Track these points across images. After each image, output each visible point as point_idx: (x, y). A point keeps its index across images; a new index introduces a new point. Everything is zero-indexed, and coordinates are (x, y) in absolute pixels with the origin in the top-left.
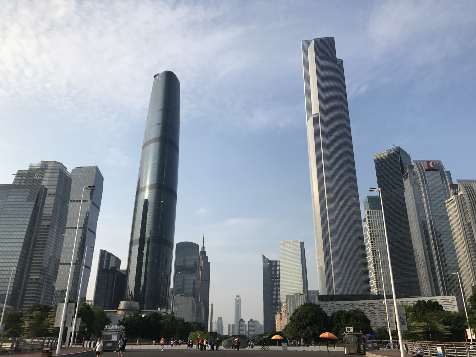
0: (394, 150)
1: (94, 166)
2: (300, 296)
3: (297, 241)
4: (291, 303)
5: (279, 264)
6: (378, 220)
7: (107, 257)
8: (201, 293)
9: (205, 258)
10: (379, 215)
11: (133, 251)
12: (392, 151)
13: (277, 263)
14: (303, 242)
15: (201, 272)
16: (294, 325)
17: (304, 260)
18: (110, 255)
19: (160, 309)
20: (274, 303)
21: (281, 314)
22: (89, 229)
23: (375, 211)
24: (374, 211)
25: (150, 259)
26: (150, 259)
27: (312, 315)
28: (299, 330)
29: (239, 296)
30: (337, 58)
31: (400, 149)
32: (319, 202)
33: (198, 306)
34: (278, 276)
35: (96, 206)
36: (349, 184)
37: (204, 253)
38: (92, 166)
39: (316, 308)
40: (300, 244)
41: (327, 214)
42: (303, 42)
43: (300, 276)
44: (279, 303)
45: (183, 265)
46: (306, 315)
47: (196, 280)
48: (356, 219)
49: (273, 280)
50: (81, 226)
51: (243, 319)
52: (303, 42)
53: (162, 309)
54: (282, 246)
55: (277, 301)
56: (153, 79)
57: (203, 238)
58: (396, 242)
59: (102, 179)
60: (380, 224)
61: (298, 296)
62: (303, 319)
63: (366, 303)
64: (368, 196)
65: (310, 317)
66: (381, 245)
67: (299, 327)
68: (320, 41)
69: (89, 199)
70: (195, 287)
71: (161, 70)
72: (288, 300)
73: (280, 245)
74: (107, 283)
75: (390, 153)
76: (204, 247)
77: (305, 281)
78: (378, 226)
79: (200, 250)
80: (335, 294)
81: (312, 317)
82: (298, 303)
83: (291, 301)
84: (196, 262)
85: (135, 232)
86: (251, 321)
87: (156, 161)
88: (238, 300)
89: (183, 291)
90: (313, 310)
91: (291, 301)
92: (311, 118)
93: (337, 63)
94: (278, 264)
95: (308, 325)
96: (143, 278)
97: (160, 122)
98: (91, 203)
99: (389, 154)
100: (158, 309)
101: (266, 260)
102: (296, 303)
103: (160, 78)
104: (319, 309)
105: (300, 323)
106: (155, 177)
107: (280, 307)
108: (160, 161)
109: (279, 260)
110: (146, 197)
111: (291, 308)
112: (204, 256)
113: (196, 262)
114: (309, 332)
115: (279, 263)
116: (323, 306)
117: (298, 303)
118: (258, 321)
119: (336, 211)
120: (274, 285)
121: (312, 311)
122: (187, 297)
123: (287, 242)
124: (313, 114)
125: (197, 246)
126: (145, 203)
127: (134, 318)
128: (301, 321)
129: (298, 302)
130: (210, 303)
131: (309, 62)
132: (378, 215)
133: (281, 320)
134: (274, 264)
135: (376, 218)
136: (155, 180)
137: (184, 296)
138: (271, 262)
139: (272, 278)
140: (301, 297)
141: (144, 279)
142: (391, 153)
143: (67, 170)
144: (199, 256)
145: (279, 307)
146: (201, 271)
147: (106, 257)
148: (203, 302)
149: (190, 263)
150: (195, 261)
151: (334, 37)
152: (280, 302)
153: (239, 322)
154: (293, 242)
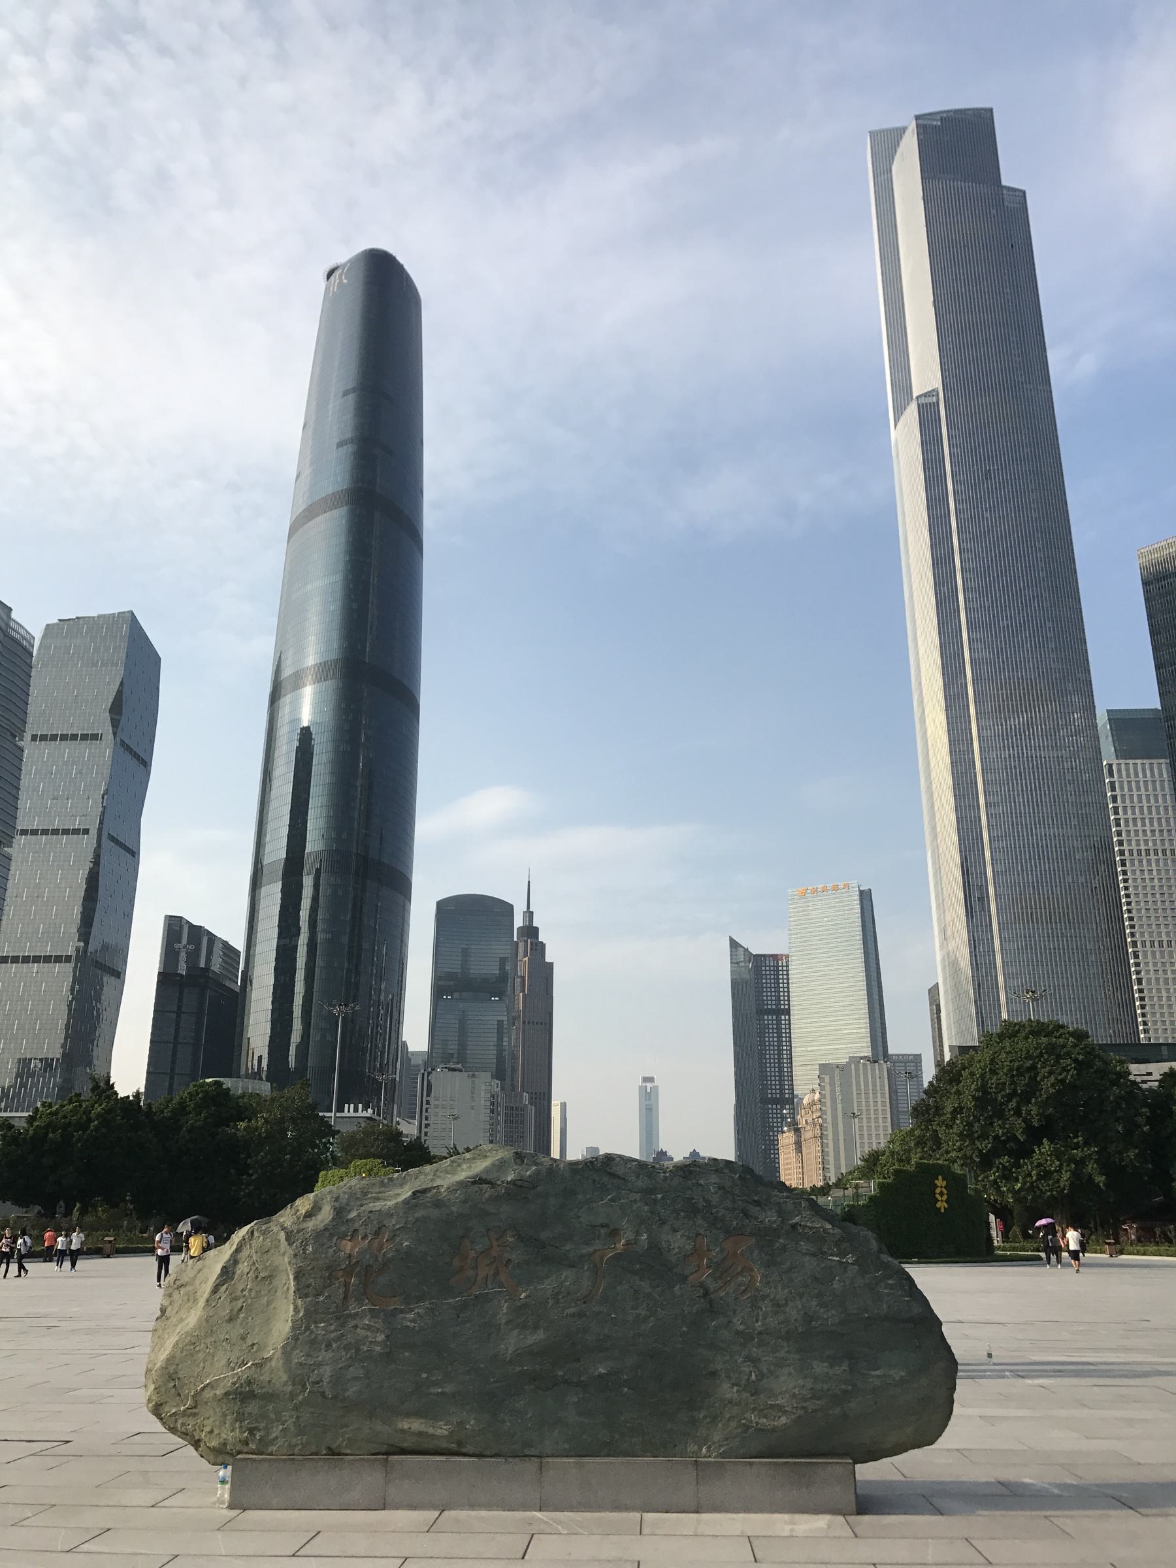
1: (121, 613)
2: (869, 1067)
3: (847, 886)
5: (787, 966)
6: (1148, 796)
7: (189, 943)
8: (523, 1064)
10: (1148, 774)
11: (263, 903)
13: (778, 963)
14: (870, 890)
15: (521, 994)
16: (961, 1135)
17: (871, 947)
18: (197, 932)
19: (352, 1106)
20: (769, 1096)
21: (797, 1131)
22: (109, 834)
23: (1134, 761)
24: (1131, 762)
25: (323, 931)
26: (323, 931)
27: (1062, 1081)
28: (986, 1162)
29: (651, 1080)
30: (1005, 182)
32: (944, 716)
33: (512, 1108)
34: (784, 1005)
35: (136, 756)
36: (1056, 648)
37: (530, 931)
38: (116, 611)
39: (1075, 1046)
40: (857, 898)
41: (973, 758)
43: (860, 1005)
44: (787, 1096)
45: (460, 971)
46: (1024, 1080)
47: (506, 1022)
48: (1086, 777)
49: (768, 1020)
50: (79, 824)
53: (360, 1106)
54: (797, 903)
55: (782, 1089)
56: (322, 283)
57: (529, 882)
59: (154, 661)
60: (1154, 809)
61: (861, 1065)
62: (1010, 1100)
63: (1150, 1074)
64: (1108, 711)
65: (1051, 1090)
66: (1159, 882)
67: (986, 1145)
68: (939, 123)
69: (106, 729)
70: (505, 1044)
71: (345, 253)
73: (789, 900)
74: (178, 1023)
76: (532, 912)
77: (878, 1025)
78: (1154, 815)
79: (518, 922)
81: (1058, 1091)
82: (863, 1092)
83: (837, 1083)
84: (503, 961)
85: (268, 838)
87: (338, 578)
89: (462, 1059)
90: (1059, 1057)
91: (837, 1083)
92: (912, 411)
93: (1006, 204)
94: (782, 966)
95: (1035, 1135)
97: (349, 435)
98: (115, 744)
100: (346, 1106)
101: (742, 953)
103: (345, 279)
104: (1093, 1049)
105: (991, 1124)
106: (335, 635)
107: (794, 1109)
108: (350, 577)
109: (785, 952)
110: (306, 719)
112: (531, 943)
113: (503, 961)
114: (1046, 1175)
115: (787, 962)
117: (863, 1092)
119: (1009, 747)
120: (771, 1035)
121: (1057, 1061)
122: (471, 1073)
123: (815, 891)
124: (915, 395)
125: (508, 909)
126: (300, 741)
127: (87, 1112)
128: (1000, 1114)
129: (862, 1087)
131: (897, 212)
132: (1145, 776)
133: (797, 1153)
134: (770, 966)
135: (1138, 789)
136: (335, 646)
137: (461, 1071)
138: (759, 959)
139: (762, 1012)
140: (873, 1070)
143: (14, 615)
144: (517, 943)
145: (789, 1109)
146: (524, 991)
147: (184, 941)
148: (532, 1093)
149: (485, 966)
150: (501, 958)
151: (991, 110)
154: (835, 888)
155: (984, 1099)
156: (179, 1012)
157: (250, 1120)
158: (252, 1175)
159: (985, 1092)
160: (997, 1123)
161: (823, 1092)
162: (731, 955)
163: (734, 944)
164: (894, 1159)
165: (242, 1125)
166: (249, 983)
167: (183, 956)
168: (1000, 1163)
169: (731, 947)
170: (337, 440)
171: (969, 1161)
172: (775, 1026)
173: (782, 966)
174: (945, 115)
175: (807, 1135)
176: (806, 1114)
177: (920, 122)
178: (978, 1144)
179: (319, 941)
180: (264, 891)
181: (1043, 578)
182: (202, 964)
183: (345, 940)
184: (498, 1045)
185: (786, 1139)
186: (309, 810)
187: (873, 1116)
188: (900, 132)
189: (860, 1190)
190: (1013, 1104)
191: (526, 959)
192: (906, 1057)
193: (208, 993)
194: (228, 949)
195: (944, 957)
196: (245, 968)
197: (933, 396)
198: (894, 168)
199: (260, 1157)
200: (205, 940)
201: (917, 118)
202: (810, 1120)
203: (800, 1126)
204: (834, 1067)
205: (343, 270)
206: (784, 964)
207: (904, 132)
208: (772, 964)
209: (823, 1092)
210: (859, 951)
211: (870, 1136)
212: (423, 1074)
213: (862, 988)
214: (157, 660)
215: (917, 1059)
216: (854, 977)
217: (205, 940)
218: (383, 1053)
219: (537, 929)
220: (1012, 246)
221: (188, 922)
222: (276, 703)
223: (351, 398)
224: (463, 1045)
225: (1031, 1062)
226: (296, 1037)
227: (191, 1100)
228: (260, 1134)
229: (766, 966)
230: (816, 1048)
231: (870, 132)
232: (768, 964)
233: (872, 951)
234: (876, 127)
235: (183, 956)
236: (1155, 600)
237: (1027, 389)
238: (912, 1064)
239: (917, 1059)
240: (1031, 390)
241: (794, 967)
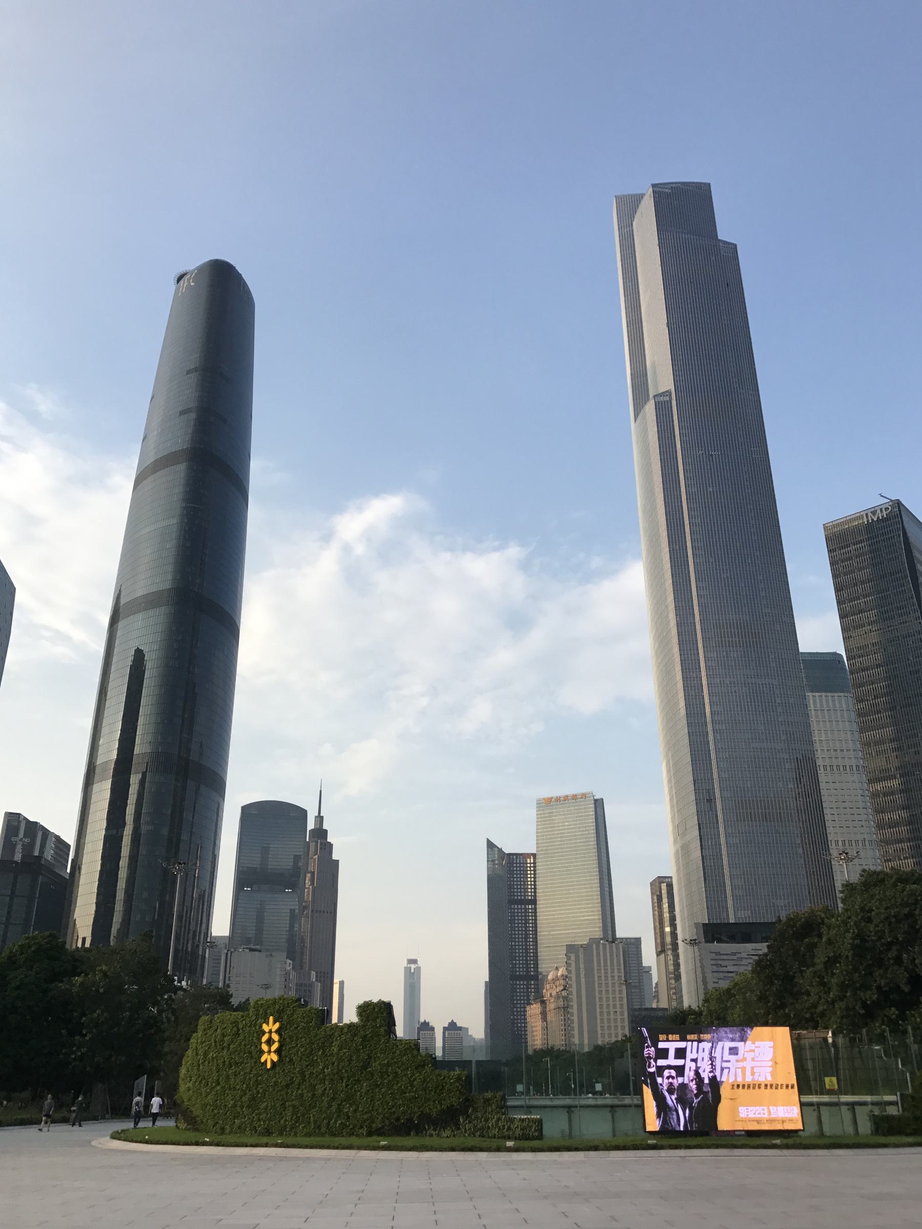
0: (884, 510)
4: (582, 966)
7: (25, 836)
9: (325, 849)
11: (94, 798)
12: (879, 511)
18: (33, 828)
21: (543, 1002)
24: (817, 694)
29: (414, 961)
30: (719, 237)
31: (902, 508)
33: (301, 985)
37: (320, 833)
40: (593, 806)
42: (620, 199)
44: (532, 973)
47: (297, 911)
51: (428, 1023)
52: (620, 199)
56: (172, 286)
57: (321, 791)
58: (898, 775)
61: (601, 946)
62: (889, 949)
70: (295, 929)
72: (573, 957)
75: (872, 520)
76: (323, 817)
79: (311, 825)
80: (732, 921)
83: (581, 960)
84: (297, 858)
86: (452, 1026)
87: (173, 521)
88: (412, 971)
91: (581, 960)
96: (121, 884)
99: (870, 521)
102: (596, 970)
103: (193, 282)
105: (871, 973)
108: (186, 521)
111: (580, 981)
112: (321, 844)
116: (725, 957)
118: (467, 1029)
125: (303, 813)
130: (336, 980)
134: (520, 863)
137: (260, 951)
140: (611, 948)
141: (124, 887)
142: (875, 519)
147: (21, 834)
152: (538, 971)
153: (419, 1029)
155: (861, 947)
156: (12, 897)
157: (87, 975)
158: (85, 1035)
159: (863, 940)
160: (878, 973)
161: (570, 968)
162: (488, 854)
163: (490, 845)
164: (712, 1017)
165: (78, 979)
166: (77, 871)
167: (19, 848)
168: (885, 1016)
169: (487, 847)
170: (180, 409)
171: (852, 1013)
172: (516, 918)
173: (530, 863)
174: (674, 185)
175: (551, 1006)
176: (550, 988)
177: (655, 189)
178: (861, 994)
179: (143, 832)
180: (96, 787)
181: (755, 540)
182: (36, 853)
183: (165, 831)
184: (289, 931)
185: (534, 1010)
186: (140, 717)
187: (610, 989)
188: (640, 197)
189: (803, 1041)
190: (893, 953)
191: (316, 856)
192: (628, 940)
193: (40, 879)
194: (62, 845)
195: (677, 850)
196: (75, 856)
197: (667, 395)
198: (634, 223)
199: (95, 1015)
200: (40, 834)
201: (654, 186)
202: (554, 993)
203: (545, 999)
204: (580, 946)
205: (191, 276)
206: (532, 861)
207: (642, 198)
208: (518, 862)
209: (570, 968)
210: (594, 850)
211: (608, 1006)
212: (227, 954)
213: (596, 881)
214: (15, 589)
215: (637, 942)
216: (589, 872)
217: (40, 834)
218: (194, 935)
219: (326, 831)
220: (727, 284)
221: (25, 818)
222: (115, 626)
223: (194, 377)
224: (259, 929)
225: (908, 909)
226: (117, 919)
227: (22, 953)
228: (97, 990)
229: (516, 863)
230: (557, 932)
231: (616, 197)
232: (518, 862)
233: (604, 851)
234: (619, 193)
235: (19, 848)
236: (838, 563)
237: (740, 393)
238: (633, 946)
239: (637, 942)
240: (743, 394)
241: (540, 864)
